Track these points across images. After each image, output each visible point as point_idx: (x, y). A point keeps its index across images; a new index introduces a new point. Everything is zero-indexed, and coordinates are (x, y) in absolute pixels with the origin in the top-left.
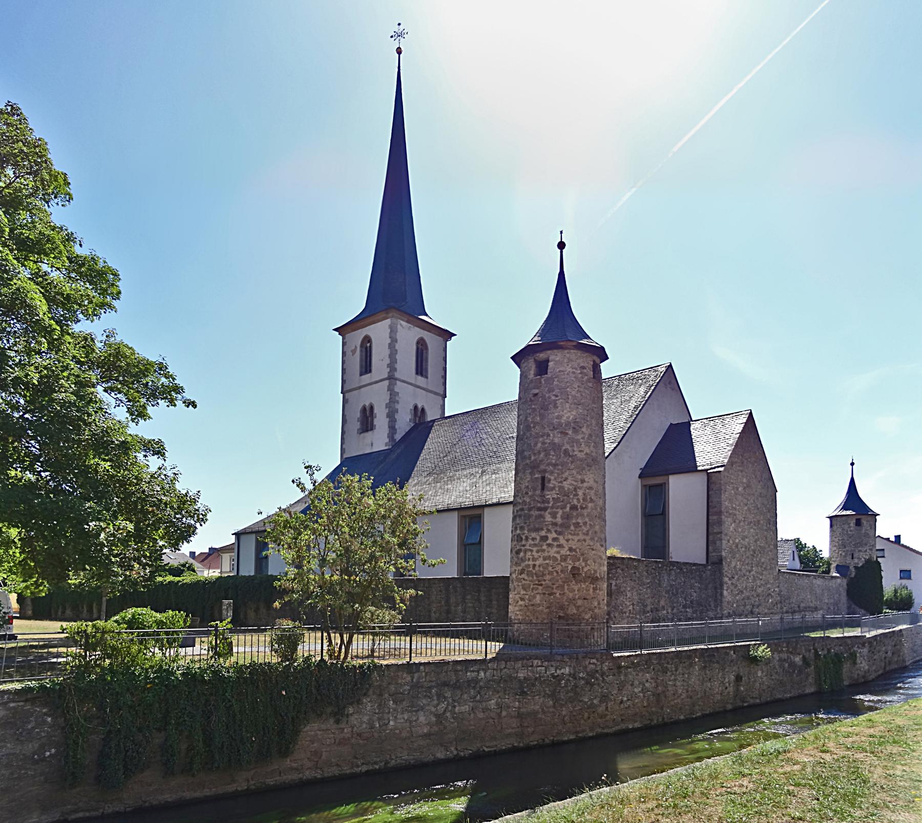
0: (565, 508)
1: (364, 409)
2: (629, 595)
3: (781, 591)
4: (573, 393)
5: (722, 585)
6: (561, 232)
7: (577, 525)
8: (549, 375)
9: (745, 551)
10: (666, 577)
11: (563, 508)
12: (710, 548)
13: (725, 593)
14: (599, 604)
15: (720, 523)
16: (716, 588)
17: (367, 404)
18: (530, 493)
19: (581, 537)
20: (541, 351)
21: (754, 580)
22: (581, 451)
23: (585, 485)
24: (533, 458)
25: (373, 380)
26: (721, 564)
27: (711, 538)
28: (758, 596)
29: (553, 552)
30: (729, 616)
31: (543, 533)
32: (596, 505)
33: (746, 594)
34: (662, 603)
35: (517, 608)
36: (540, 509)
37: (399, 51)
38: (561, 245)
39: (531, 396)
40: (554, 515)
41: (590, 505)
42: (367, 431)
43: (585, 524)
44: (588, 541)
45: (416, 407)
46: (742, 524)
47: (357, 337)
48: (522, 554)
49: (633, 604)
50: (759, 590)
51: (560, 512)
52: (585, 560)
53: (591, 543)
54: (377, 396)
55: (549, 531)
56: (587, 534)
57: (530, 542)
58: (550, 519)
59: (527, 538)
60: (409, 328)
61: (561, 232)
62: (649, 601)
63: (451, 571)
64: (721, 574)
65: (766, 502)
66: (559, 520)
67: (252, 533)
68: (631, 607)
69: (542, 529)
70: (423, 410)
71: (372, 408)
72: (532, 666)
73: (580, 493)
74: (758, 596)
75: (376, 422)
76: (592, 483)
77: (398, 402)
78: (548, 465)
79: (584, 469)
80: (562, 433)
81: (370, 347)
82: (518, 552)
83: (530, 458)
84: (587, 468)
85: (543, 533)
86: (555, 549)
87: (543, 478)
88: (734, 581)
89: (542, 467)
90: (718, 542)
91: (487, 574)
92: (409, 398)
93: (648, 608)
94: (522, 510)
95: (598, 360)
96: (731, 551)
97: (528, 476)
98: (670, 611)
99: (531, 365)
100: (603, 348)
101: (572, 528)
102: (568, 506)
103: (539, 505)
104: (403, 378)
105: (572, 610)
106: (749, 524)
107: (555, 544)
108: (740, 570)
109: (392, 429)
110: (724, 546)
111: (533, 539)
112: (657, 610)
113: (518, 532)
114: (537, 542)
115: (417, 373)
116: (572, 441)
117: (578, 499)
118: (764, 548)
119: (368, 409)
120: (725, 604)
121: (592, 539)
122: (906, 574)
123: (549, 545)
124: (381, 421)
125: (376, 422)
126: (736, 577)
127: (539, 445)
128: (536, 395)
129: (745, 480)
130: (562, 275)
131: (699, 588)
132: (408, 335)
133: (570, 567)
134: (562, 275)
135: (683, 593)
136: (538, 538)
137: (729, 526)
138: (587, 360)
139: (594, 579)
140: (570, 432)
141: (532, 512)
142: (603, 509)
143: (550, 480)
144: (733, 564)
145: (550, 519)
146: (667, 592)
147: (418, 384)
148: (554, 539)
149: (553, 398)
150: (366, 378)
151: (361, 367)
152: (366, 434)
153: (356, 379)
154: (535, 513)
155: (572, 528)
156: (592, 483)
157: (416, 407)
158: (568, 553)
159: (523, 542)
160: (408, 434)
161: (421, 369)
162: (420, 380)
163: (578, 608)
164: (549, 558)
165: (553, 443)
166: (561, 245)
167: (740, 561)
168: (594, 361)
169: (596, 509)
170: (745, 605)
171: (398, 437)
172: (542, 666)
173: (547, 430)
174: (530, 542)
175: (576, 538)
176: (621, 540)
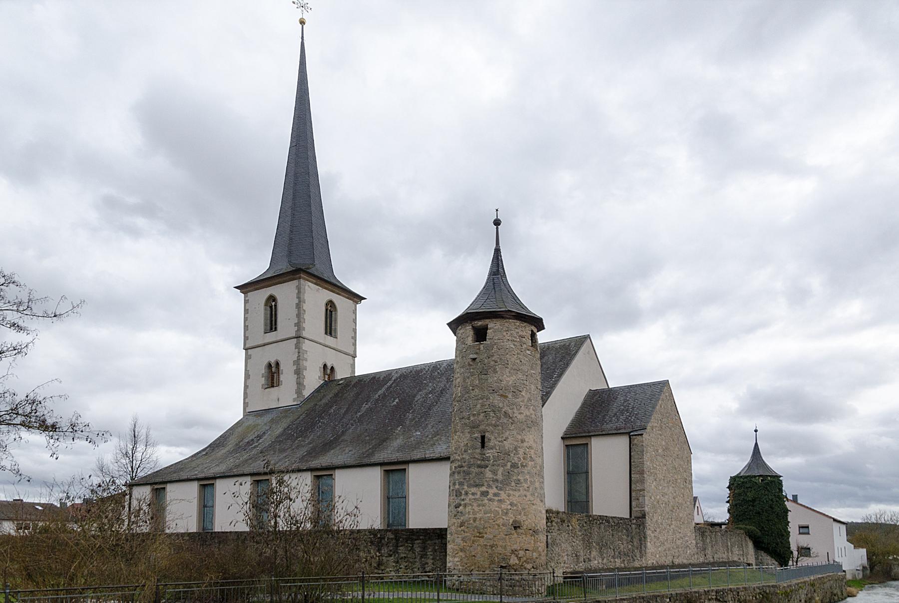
0: (506, 465)
4: (513, 360)
7: (518, 482)
8: (488, 342)
11: (504, 465)
12: (634, 503)
15: (642, 481)
19: (522, 492)
20: (480, 319)
21: (674, 533)
22: (520, 413)
23: (525, 444)
24: (472, 418)
25: (279, 338)
27: (633, 494)
29: (494, 506)
31: (484, 489)
33: (667, 545)
36: (479, 466)
37: (302, 22)
40: (495, 473)
42: (273, 386)
43: (526, 480)
44: (529, 497)
45: (325, 366)
47: (262, 295)
51: (501, 470)
54: (284, 354)
55: (489, 486)
57: (470, 496)
58: (491, 476)
59: (467, 494)
60: (317, 290)
63: (193, 528)
65: (682, 463)
66: (500, 477)
67: (147, 484)
69: (483, 485)
70: (332, 368)
71: (277, 364)
73: (521, 451)
76: (531, 442)
77: (306, 360)
78: (488, 425)
80: (502, 395)
81: (275, 306)
83: (469, 419)
84: (527, 429)
85: (484, 489)
86: (496, 503)
87: (483, 438)
88: (656, 534)
89: (482, 427)
91: (217, 529)
92: (316, 357)
95: (535, 330)
96: (654, 507)
97: (468, 435)
99: (468, 331)
100: (541, 320)
101: (513, 484)
102: (509, 464)
103: (479, 462)
104: (310, 338)
105: (514, 561)
107: (496, 498)
109: (300, 385)
110: (647, 502)
111: (473, 494)
112: (590, 560)
113: (457, 486)
114: (478, 496)
115: (326, 333)
116: (511, 404)
118: (682, 504)
120: (649, 555)
121: (533, 495)
122: (805, 530)
123: (490, 500)
124: (287, 376)
125: (282, 378)
127: (479, 406)
128: (474, 359)
130: (497, 251)
132: (316, 297)
133: (511, 521)
134: (497, 251)
136: (479, 493)
137: (650, 484)
138: (526, 330)
139: (535, 532)
140: (510, 396)
141: (472, 469)
142: (542, 467)
143: (489, 440)
145: (491, 476)
146: (598, 544)
147: (327, 344)
148: (495, 495)
149: (492, 363)
151: (266, 325)
152: (272, 389)
153: (260, 337)
154: (474, 470)
155: (513, 484)
156: (531, 442)
157: (325, 366)
158: (509, 507)
160: (318, 391)
161: (330, 329)
162: (329, 340)
163: (519, 559)
164: (491, 512)
165: (492, 406)
169: (536, 467)
171: (307, 393)
173: (486, 393)
174: (470, 496)
175: (517, 493)
176: (553, 494)
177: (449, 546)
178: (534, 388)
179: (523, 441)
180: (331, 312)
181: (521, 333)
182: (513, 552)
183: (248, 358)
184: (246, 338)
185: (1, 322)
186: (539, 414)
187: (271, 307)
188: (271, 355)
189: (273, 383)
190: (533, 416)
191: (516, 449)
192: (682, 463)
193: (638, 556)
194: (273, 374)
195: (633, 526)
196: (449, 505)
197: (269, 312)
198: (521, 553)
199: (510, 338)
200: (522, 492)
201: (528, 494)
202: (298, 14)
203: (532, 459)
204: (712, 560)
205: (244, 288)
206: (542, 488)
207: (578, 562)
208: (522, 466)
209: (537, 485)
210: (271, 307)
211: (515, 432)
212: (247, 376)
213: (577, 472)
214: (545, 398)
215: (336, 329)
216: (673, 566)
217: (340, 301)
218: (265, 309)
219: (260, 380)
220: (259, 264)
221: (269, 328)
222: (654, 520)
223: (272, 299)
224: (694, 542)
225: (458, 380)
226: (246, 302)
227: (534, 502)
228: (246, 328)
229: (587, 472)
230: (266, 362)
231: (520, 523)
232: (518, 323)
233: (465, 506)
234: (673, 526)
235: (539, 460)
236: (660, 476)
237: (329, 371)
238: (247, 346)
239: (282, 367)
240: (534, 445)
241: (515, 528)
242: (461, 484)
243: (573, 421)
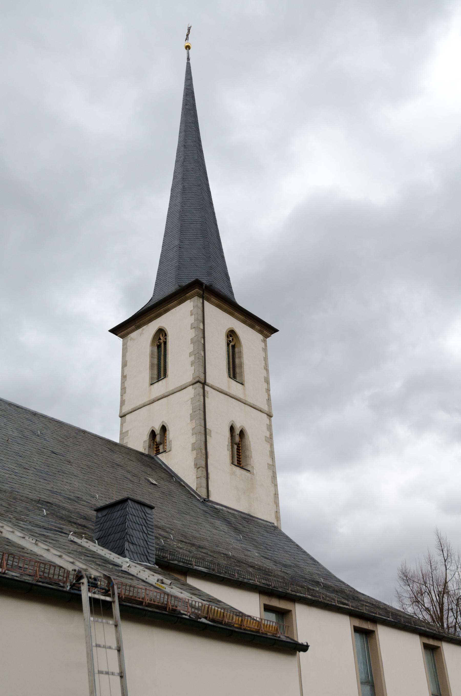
47: (145, 335)
150: (161, 387)
157: (232, 429)
162: (234, 387)
184: (122, 403)
205: (120, 330)
217: (248, 336)
223: (161, 332)
238: (126, 409)
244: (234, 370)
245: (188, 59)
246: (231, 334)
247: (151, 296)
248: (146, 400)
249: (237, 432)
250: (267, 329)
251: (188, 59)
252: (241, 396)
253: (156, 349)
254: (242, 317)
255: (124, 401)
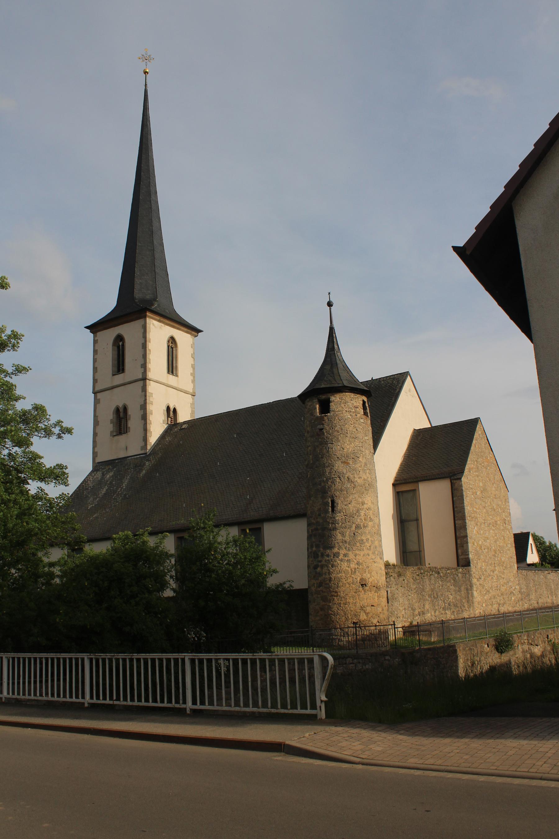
1: (117, 410)
2: (401, 600)
3: (521, 589)
5: (471, 586)
6: (329, 293)
9: (488, 552)
10: (428, 582)
12: (459, 551)
13: (475, 594)
14: (383, 610)
15: (464, 527)
16: (467, 590)
17: (121, 406)
18: (322, 515)
22: (360, 478)
23: (365, 506)
26: (470, 566)
27: (459, 541)
28: (502, 594)
30: (471, 640)
32: (374, 524)
33: (493, 593)
34: (427, 606)
35: (318, 618)
38: (330, 304)
39: (318, 430)
41: (370, 523)
46: (482, 526)
47: (109, 335)
48: (319, 569)
49: (405, 609)
50: (503, 589)
52: (370, 573)
53: (373, 557)
56: (370, 549)
58: (341, 538)
61: (329, 293)
62: (416, 605)
64: (470, 575)
65: (500, 503)
68: (403, 612)
70: (175, 410)
71: (125, 408)
72: (346, 663)
74: (502, 594)
75: (131, 424)
76: (370, 504)
79: (363, 493)
81: (123, 345)
82: (316, 567)
83: (320, 484)
88: (481, 582)
90: (465, 545)
93: (416, 612)
94: (317, 529)
98: (433, 613)
101: (358, 544)
102: (354, 526)
105: (363, 617)
106: (488, 526)
108: (486, 571)
112: (424, 613)
115: (168, 372)
117: (361, 519)
119: (121, 410)
120: (476, 604)
121: (374, 553)
123: (341, 560)
125: (130, 424)
126: (483, 578)
129: (481, 484)
130: (332, 330)
131: (455, 591)
132: (158, 332)
133: (359, 579)
134: (332, 330)
135: (442, 595)
139: (378, 588)
140: (351, 462)
142: (379, 525)
144: (479, 564)
145: (341, 538)
146: (430, 596)
148: (345, 555)
150: (119, 379)
153: (107, 380)
157: (168, 408)
158: (356, 567)
159: (320, 559)
162: (171, 380)
166: (330, 304)
167: (485, 561)
168: (363, 401)
169: (374, 527)
170: (492, 605)
172: (353, 663)
176: (390, 552)
177: (312, 607)
178: (363, 426)
179: (363, 503)
180: (172, 348)
181: (355, 404)
182: (362, 608)
183: (97, 402)
184: (95, 381)
185: (1, 438)
186: (374, 476)
187: (118, 347)
188: (118, 398)
189: (120, 429)
190: (369, 479)
191: (358, 511)
192: (500, 503)
193: (466, 606)
194: (121, 420)
195: (460, 575)
196: (309, 567)
197: (116, 353)
198: (368, 609)
199: (347, 409)
200: (366, 552)
201: (370, 552)
202: (142, 66)
203: (371, 520)
204: (536, 605)
205: (94, 328)
206: (381, 546)
207: (414, 615)
208: (364, 526)
209: (376, 543)
210: (118, 347)
211: (356, 496)
212: (96, 423)
213: (407, 521)
214: (374, 454)
215: (176, 367)
216: (469, 618)
217: (183, 338)
218: (113, 350)
219: (107, 427)
220: (107, 301)
221: (116, 369)
222: (479, 566)
223: (120, 339)
224: (517, 587)
225: (310, 448)
226: (95, 342)
227: (376, 560)
228: (95, 369)
229: (417, 520)
230: (113, 407)
231: (365, 580)
232: (352, 395)
233: (322, 567)
234: (496, 572)
235: (376, 521)
236: (481, 520)
237: (171, 413)
238: (97, 389)
239: (130, 412)
240: (372, 506)
241: (362, 585)
242: (317, 546)
243: (402, 465)
244: (172, 368)
245: (146, 85)
246: (172, 340)
247: (114, 304)
248: (109, 385)
249: (172, 409)
250: (194, 330)
251: (146, 85)
252: (175, 385)
253: (116, 348)
254: (186, 329)
255: (97, 380)
